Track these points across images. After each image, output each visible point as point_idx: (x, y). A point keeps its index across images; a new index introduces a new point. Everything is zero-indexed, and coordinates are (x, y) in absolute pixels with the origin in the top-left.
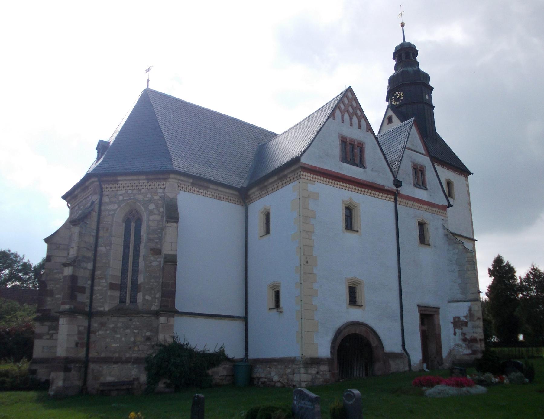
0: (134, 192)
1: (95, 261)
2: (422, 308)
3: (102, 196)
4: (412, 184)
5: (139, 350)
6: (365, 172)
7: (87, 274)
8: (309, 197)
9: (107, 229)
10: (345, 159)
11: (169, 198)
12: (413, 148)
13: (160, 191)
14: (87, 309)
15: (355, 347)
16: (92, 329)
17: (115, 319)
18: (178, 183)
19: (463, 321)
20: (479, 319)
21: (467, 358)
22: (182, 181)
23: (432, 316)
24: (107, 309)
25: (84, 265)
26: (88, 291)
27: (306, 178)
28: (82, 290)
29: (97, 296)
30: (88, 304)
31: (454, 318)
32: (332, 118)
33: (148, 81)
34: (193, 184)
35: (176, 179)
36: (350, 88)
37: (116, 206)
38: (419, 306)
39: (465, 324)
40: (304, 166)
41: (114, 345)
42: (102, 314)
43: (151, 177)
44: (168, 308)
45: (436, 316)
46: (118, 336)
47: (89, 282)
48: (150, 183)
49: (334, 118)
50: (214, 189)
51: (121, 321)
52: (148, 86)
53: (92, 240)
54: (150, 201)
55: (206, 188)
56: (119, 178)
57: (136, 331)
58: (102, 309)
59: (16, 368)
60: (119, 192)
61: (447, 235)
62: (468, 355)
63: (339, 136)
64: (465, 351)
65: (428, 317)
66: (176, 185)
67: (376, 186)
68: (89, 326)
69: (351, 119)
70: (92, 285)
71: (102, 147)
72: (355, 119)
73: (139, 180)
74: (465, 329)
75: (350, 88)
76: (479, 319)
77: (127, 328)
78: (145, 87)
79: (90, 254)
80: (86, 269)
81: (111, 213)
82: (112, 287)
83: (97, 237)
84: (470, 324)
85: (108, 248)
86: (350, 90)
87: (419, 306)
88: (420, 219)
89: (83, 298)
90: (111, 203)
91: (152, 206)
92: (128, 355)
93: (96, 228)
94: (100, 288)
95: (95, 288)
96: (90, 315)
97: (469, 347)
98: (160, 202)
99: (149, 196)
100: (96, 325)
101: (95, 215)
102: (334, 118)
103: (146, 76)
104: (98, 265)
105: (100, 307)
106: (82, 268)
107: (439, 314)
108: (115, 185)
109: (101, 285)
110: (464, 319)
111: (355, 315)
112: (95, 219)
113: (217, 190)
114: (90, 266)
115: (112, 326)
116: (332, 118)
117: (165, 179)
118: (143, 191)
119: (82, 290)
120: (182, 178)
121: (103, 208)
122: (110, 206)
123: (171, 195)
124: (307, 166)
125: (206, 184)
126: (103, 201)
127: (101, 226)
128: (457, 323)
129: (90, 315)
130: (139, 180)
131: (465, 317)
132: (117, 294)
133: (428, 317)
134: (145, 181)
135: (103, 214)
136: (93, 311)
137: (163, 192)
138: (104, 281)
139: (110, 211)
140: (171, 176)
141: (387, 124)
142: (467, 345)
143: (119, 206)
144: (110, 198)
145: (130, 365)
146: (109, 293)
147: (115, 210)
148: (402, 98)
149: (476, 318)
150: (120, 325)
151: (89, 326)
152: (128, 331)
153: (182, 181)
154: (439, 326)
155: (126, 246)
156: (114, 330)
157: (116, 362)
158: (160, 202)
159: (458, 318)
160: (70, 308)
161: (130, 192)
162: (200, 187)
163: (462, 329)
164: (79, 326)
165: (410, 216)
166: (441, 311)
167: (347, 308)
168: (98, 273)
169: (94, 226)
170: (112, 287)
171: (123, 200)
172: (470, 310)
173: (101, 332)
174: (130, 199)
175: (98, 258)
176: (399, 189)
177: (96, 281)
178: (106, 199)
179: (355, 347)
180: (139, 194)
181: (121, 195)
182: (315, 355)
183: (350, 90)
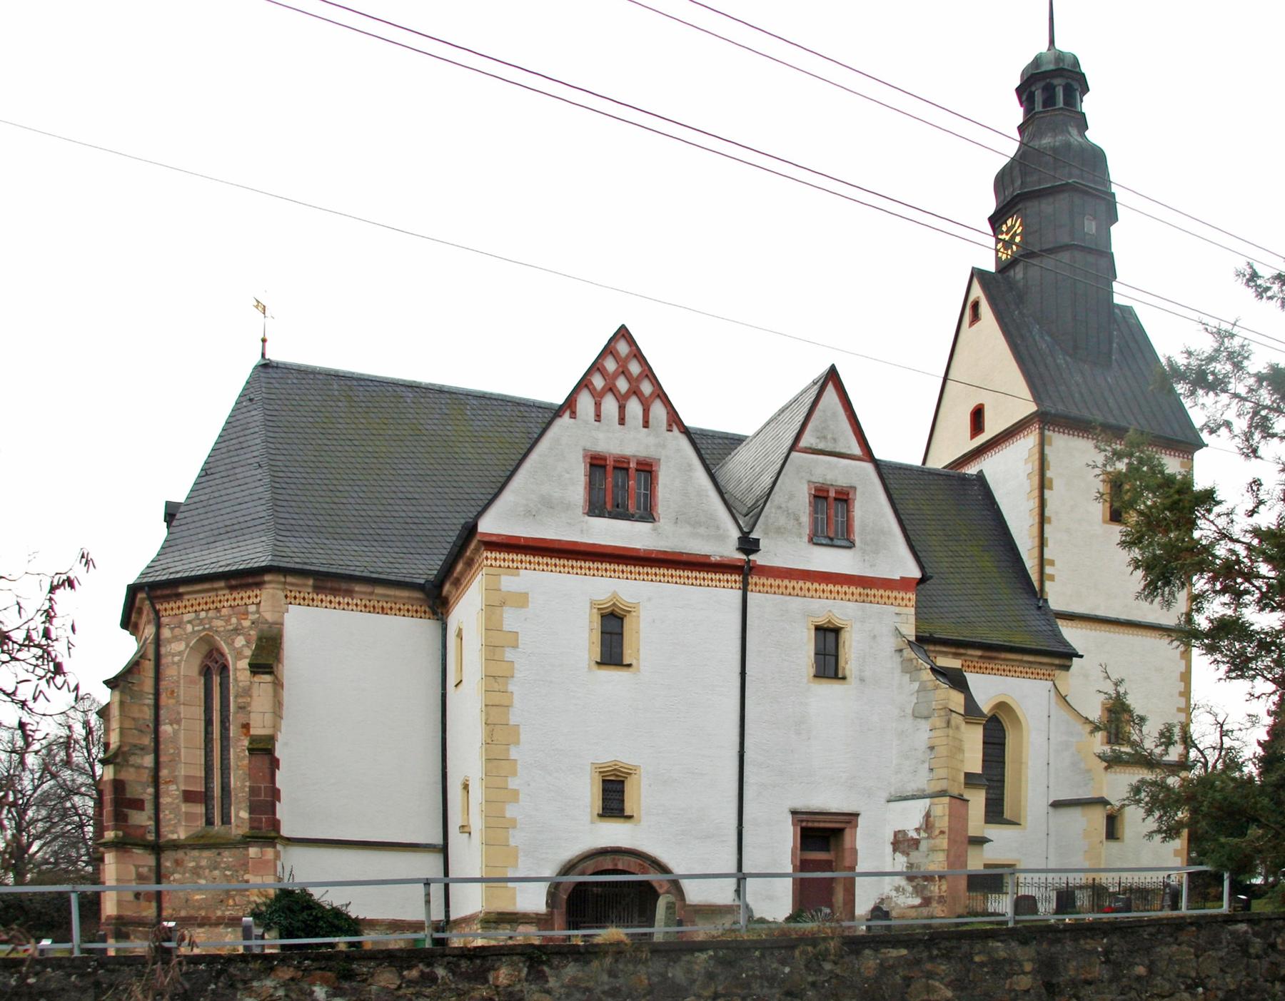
0: (211, 614)
1: (157, 751)
2: (804, 817)
3: (159, 626)
4: (806, 539)
5: (235, 905)
6: (655, 530)
7: (146, 776)
8: (503, 604)
9: (173, 692)
10: (596, 508)
11: (266, 622)
12: (821, 446)
13: (252, 608)
14: (151, 837)
15: (608, 892)
16: (163, 871)
17: (196, 853)
18: (283, 590)
19: (913, 839)
20: (942, 832)
21: (913, 913)
22: (292, 584)
23: (841, 830)
24: (183, 836)
25: (135, 760)
26: (149, 807)
27: (498, 563)
28: (138, 804)
29: (166, 815)
30: (153, 828)
31: (896, 834)
32: (567, 414)
33: (264, 341)
34: (317, 589)
35: (278, 583)
36: (623, 328)
37: (182, 646)
38: (794, 813)
39: (916, 843)
40: (486, 539)
41: (197, 897)
42: (176, 846)
43: (233, 582)
44: (266, 832)
45: (847, 832)
46: (203, 882)
47: (151, 790)
48: (235, 595)
49: (573, 415)
50: (364, 593)
51: (205, 857)
52: (263, 355)
53: (148, 714)
54: (237, 631)
55: (349, 593)
56: (181, 590)
57: (228, 873)
58: (175, 837)
59: (280, 974)
60: (186, 617)
61: (901, 651)
62: (913, 907)
63: (585, 457)
64: (905, 900)
65: (822, 836)
66: (281, 594)
67: (684, 558)
68: (159, 865)
69: (622, 409)
70: (157, 796)
71: (171, 513)
72: (634, 407)
73: (216, 590)
74: (916, 856)
75: (623, 328)
76: (942, 832)
77: (215, 868)
78: (257, 359)
79: (147, 741)
80: (139, 767)
81: (176, 659)
82: (189, 797)
83: (157, 707)
84: (924, 845)
85: (176, 726)
86: (623, 333)
87: (794, 813)
88: (822, 621)
89: (142, 818)
90: (175, 638)
91: (240, 641)
92: (219, 913)
93: (152, 691)
94: (169, 800)
95: (162, 800)
96: (157, 848)
97: (918, 891)
98: (252, 633)
99: (234, 620)
100: (168, 864)
101: (149, 666)
102: (573, 415)
103: (254, 325)
104: (163, 759)
105: (173, 832)
106: (133, 766)
107: (856, 826)
108: (179, 603)
109: (170, 796)
110: (915, 836)
111: (614, 834)
112: (151, 674)
113: (372, 593)
114: (148, 761)
115: (192, 864)
116: (567, 414)
117: (259, 585)
118: (224, 611)
119: (138, 804)
120: (290, 579)
121: (163, 650)
122: (173, 645)
123: (269, 616)
124: (494, 539)
125: (344, 586)
126: (162, 637)
127: (163, 684)
128: (901, 843)
129: (157, 848)
130: (216, 590)
131: (917, 830)
132: (200, 809)
133: (822, 836)
134: (226, 592)
135: (164, 661)
136: (162, 840)
137: (258, 612)
138: (174, 787)
139: (174, 655)
140: (267, 578)
141: (971, 325)
142: (914, 887)
143: (187, 646)
144: (172, 629)
145: (221, 929)
146: (184, 808)
147: (180, 653)
148: (1018, 239)
149: (937, 832)
150: (204, 863)
151: (159, 865)
152: (216, 873)
153: (292, 584)
154: (854, 851)
155: (208, 722)
156: (196, 872)
157: (201, 925)
158: (252, 633)
159: (904, 832)
160: (116, 836)
161: (203, 614)
162: (335, 592)
163: (908, 854)
164: (137, 867)
165: (786, 622)
166: (861, 821)
167: (592, 822)
168: (164, 773)
169: (148, 686)
170: (189, 797)
171: (194, 632)
172: (928, 815)
173: (177, 876)
174: (204, 629)
175: (162, 747)
176: (752, 557)
177: (162, 787)
178: (166, 633)
179: (608, 892)
180: (217, 618)
181: (189, 622)
182: (508, 908)
183: (623, 333)
